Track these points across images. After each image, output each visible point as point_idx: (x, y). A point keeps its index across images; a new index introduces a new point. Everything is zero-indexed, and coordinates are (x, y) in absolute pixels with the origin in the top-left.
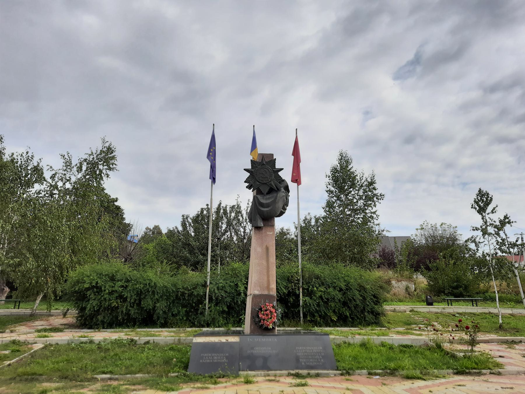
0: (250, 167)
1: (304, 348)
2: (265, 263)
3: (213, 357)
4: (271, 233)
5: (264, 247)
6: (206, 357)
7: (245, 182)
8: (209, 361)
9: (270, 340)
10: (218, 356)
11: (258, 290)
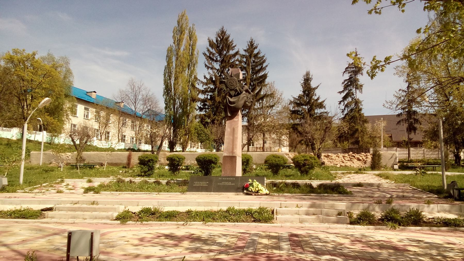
2: (231, 137)
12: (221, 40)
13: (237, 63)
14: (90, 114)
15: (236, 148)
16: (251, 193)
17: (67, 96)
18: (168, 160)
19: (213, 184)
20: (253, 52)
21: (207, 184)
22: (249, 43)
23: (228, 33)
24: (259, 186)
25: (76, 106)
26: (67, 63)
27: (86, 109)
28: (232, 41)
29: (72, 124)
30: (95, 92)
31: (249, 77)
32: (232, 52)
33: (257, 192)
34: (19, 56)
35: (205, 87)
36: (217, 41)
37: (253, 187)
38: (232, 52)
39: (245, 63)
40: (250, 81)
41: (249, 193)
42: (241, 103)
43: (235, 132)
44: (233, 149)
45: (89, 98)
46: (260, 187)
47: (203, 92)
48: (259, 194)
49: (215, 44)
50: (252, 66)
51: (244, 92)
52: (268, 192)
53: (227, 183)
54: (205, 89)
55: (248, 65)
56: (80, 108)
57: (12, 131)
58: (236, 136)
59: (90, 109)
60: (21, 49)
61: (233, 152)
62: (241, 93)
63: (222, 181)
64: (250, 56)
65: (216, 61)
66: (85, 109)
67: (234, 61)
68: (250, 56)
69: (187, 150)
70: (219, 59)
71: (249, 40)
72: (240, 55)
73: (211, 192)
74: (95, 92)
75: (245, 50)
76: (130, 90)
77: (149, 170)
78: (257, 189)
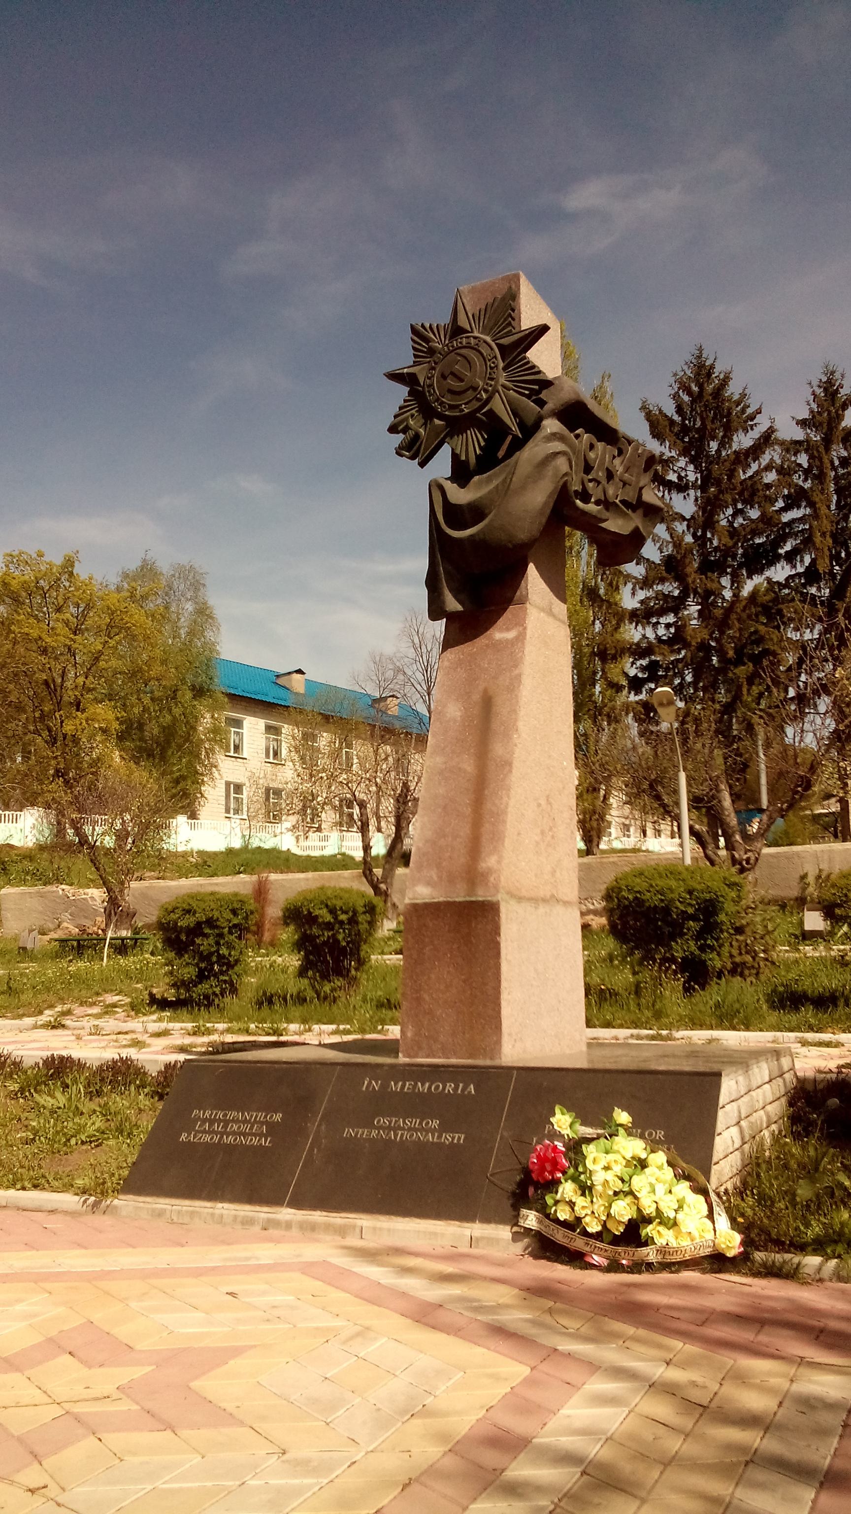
0: (403, 358)
1: (220, 1115)
2: (468, 765)
3: (225, 1127)
4: (511, 635)
5: (476, 697)
6: (204, 1121)
7: (393, 429)
8: (207, 1138)
9: (450, 1087)
10: (245, 1121)
11: (429, 883)
12: (696, 399)
13: (771, 477)
14: (284, 746)
15: (497, 837)
16: (579, 1243)
17: (199, 692)
18: (286, 924)
19: (313, 1127)
20: (840, 418)
21: (272, 1128)
22: (820, 392)
23: (719, 369)
24: (639, 1182)
25: (238, 723)
26: (197, 586)
27: (270, 729)
28: (743, 395)
29: (228, 784)
30: (300, 672)
31: (827, 526)
32: (743, 441)
33: (633, 1234)
34: (29, 575)
35: (642, 595)
36: (679, 410)
37: (586, 1189)
38: (743, 441)
39: (807, 472)
40: (830, 541)
41: (560, 1236)
42: (537, 498)
43: (495, 725)
44: (475, 849)
45: (282, 693)
46: (658, 1185)
47: (642, 616)
48: (650, 1254)
49: (672, 422)
50: (837, 478)
51: (551, 425)
52: (731, 1241)
53: (408, 1130)
54: (642, 602)
55: (820, 478)
56: (253, 728)
57: (21, 821)
58: (498, 749)
59: (286, 729)
60: (31, 551)
61: (473, 875)
62: (530, 429)
63: (384, 1103)
64: (827, 442)
65: (681, 487)
66: (269, 729)
67: (757, 473)
68: (827, 442)
69: (603, 846)
70: (692, 476)
71: (818, 376)
72: (782, 443)
73: (275, 1200)
74: (300, 672)
75: (803, 423)
76: (411, 653)
77: (202, 977)
78: (623, 1211)
